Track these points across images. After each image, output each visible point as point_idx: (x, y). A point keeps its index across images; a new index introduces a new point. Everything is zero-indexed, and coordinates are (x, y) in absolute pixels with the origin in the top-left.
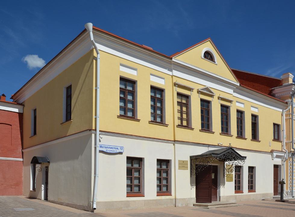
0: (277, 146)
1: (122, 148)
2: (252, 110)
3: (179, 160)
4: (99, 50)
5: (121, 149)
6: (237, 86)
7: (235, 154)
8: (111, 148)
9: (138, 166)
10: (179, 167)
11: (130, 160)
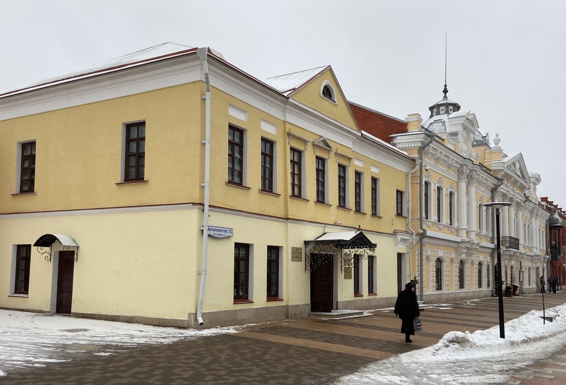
0: (400, 224)
1: (231, 230)
2: (356, 164)
3: (292, 247)
4: (210, 85)
5: (230, 231)
6: (359, 136)
7: (365, 241)
8: (219, 231)
9: (22, 256)
10: (292, 257)
11: (238, 246)
